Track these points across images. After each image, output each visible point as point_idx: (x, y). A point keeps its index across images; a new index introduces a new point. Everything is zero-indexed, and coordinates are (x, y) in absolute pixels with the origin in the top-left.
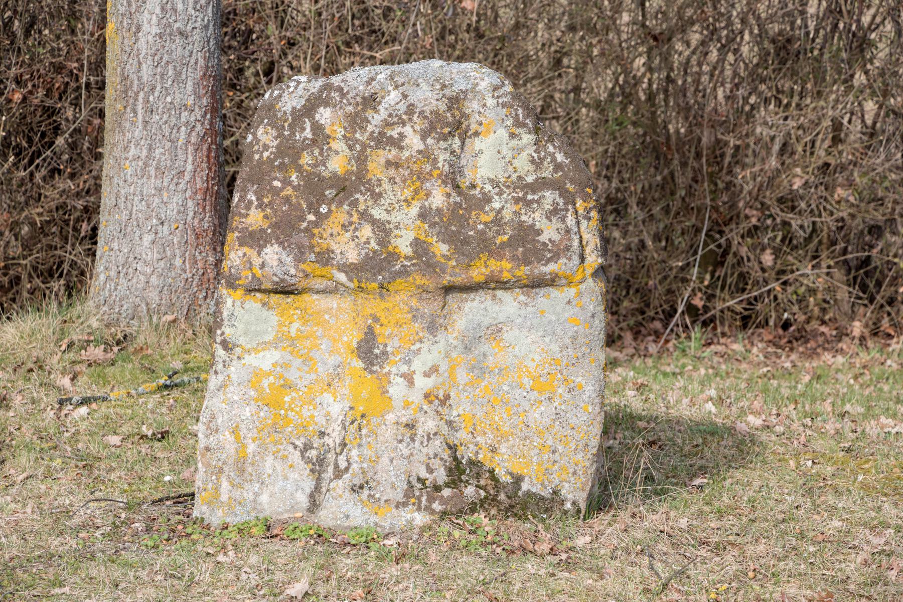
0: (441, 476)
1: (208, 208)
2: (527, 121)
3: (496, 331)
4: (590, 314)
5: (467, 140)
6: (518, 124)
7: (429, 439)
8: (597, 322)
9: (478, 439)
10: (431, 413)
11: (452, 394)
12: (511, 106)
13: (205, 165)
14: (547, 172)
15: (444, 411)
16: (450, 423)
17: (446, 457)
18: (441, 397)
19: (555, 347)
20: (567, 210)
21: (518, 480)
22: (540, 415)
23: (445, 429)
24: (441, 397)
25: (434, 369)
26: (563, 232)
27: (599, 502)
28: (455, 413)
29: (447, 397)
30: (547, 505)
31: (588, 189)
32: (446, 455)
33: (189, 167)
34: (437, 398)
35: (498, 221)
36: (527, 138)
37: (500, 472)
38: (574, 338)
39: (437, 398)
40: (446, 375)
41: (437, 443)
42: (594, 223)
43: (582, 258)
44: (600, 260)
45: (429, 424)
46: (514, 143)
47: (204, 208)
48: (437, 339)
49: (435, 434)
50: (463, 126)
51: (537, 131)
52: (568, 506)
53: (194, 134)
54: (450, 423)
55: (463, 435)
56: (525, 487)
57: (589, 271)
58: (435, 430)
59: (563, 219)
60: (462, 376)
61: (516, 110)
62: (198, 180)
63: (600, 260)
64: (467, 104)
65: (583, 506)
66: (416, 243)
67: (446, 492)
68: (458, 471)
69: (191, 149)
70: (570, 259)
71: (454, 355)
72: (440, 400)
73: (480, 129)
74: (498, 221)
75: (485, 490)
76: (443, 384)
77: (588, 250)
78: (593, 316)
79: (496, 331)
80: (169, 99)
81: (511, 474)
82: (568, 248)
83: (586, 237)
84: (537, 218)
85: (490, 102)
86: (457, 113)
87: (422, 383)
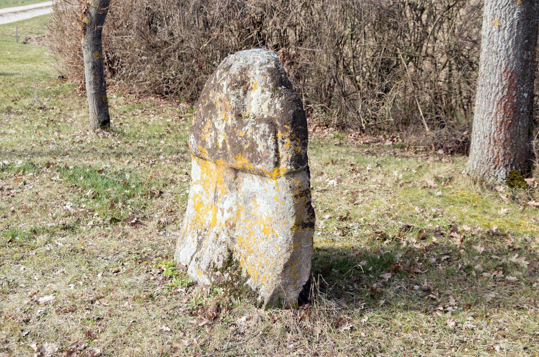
0: (220, 265)
1: (503, 130)
2: (270, 84)
3: (253, 196)
4: (283, 197)
5: (248, 92)
6: (266, 86)
7: (220, 244)
8: (287, 202)
9: (242, 250)
10: (225, 231)
11: (237, 224)
12: (265, 75)
13: (502, 111)
14: (271, 114)
15: (231, 232)
16: (232, 239)
17: (225, 255)
18: (231, 224)
19: (270, 211)
20: (269, 136)
21: (248, 277)
22: (262, 245)
23: (229, 241)
24: (231, 224)
25: (230, 210)
26: (265, 147)
27: (276, 301)
28: (236, 234)
29: (234, 225)
30: (253, 294)
31: (286, 126)
32: (226, 254)
33: (494, 111)
34: (229, 224)
35: (245, 137)
36: (268, 94)
37: (244, 270)
38: (277, 208)
39: (229, 224)
40: (235, 213)
41: (223, 247)
42: (286, 146)
43: (277, 164)
44: (289, 167)
45: (223, 237)
46: (263, 95)
47: (500, 130)
48: (233, 194)
49: (224, 242)
50: (247, 84)
51: (273, 90)
52: (259, 299)
53: (498, 96)
54: (232, 239)
55: (236, 247)
56: (248, 282)
57: (282, 173)
58: (224, 240)
59: (266, 141)
60: (243, 216)
61: (267, 77)
62: (498, 117)
63: (289, 167)
64: (249, 72)
65: (266, 301)
66: (224, 142)
67: (218, 273)
68: (230, 262)
69: (496, 103)
70: (267, 163)
71: (240, 204)
72: (230, 226)
73: (253, 86)
74: (245, 137)
75: (232, 277)
76: (233, 218)
77: (282, 161)
78: (285, 198)
79: (253, 196)
80: (488, 81)
81: (247, 273)
82: (267, 157)
83: (281, 153)
84: (257, 138)
85: (258, 72)
86: (243, 76)
87: (227, 215)
